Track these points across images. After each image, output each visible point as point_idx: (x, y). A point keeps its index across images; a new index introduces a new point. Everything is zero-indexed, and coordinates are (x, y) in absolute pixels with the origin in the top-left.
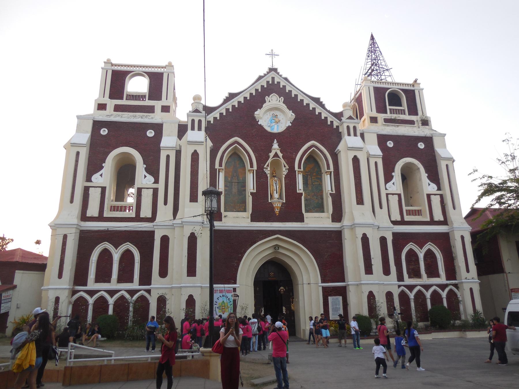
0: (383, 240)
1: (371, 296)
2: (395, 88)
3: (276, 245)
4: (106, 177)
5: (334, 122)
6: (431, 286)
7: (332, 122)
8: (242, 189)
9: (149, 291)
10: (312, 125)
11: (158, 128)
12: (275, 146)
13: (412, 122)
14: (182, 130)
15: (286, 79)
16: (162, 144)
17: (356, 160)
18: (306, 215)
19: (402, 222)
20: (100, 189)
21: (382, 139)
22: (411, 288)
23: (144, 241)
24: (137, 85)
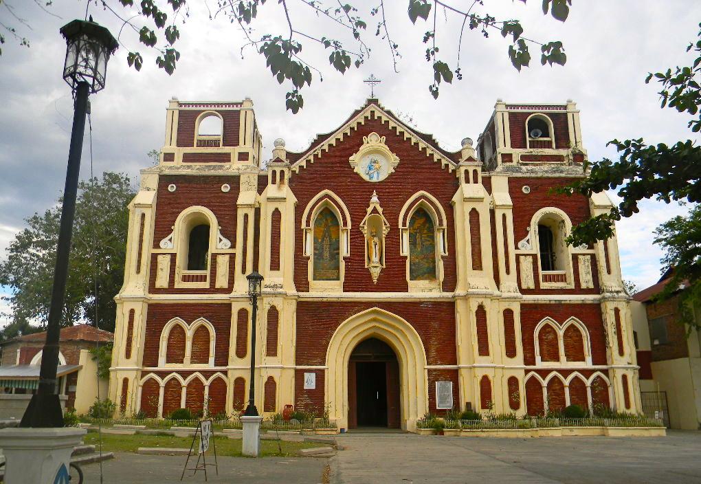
0: (508, 314)
2: (538, 112)
4: (176, 242)
5: (450, 165)
6: (571, 371)
7: (447, 166)
8: (335, 252)
9: (225, 373)
10: (423, 167)
11: (235, 181)
12: (375, 199)
13: (559, 158)
14: (262, 183)
15: (389, 113)
16: (238, 203)
17: (474, 214)
18: (411, 283)
19: (537, 290)
20: (169, 257)
21: (515, 185)
22: (544, 373)
23: (219, 314)
24: (210, 127)
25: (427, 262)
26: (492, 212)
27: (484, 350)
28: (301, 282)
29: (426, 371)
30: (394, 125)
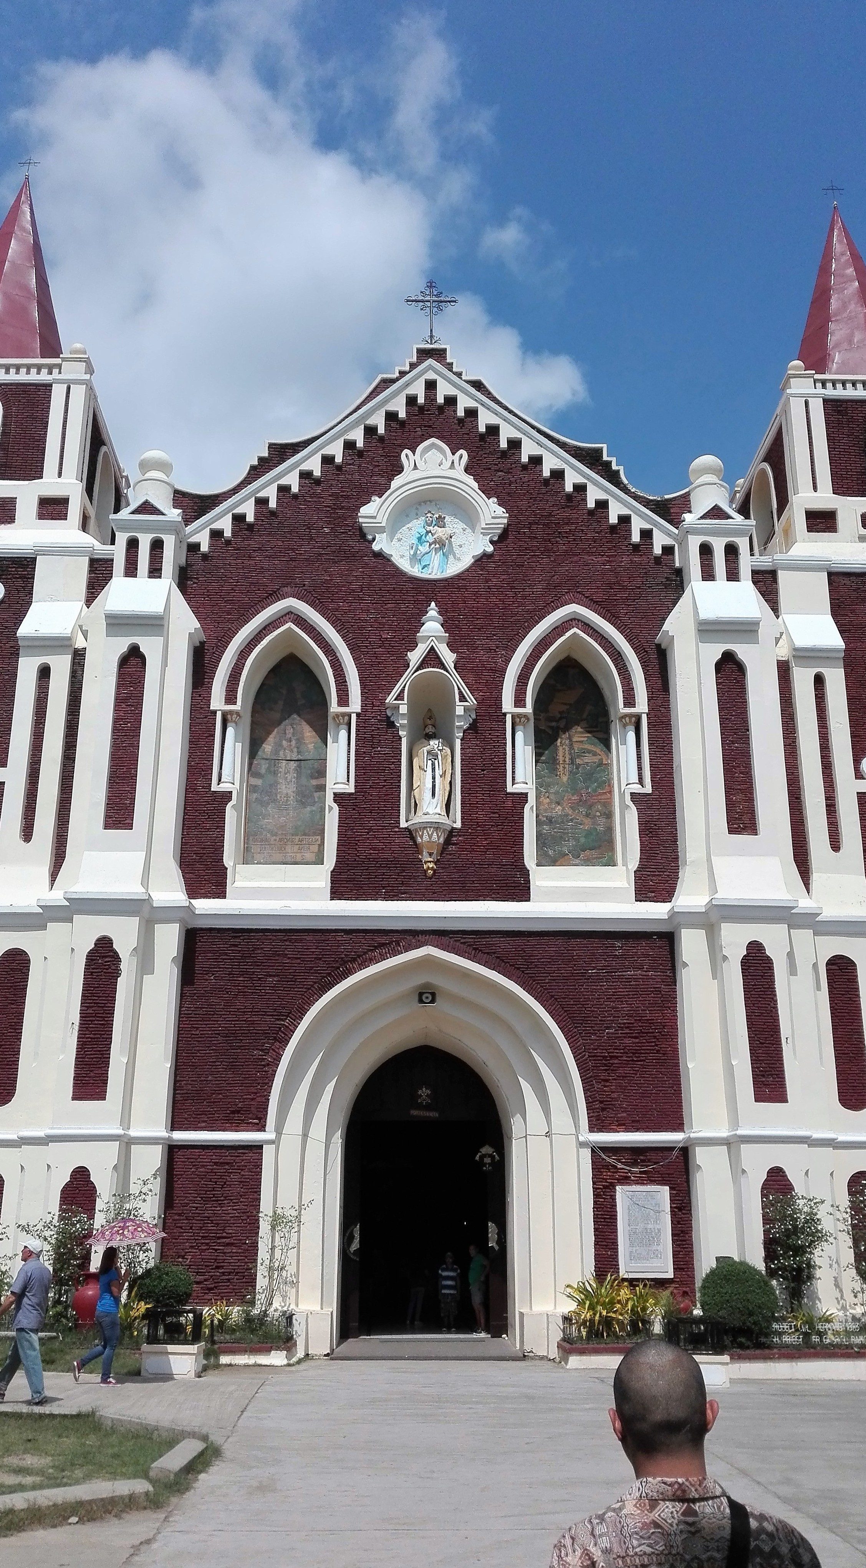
1: (777, 1183)
3: (427, 985)
8: (314, 782)
12: (432, 627)
15: (478, 385)
16: (27, 628)
17: (730, 670)
25: (587, 815)
26: (784, 670)
27: (769, 1082)
28: (203, 869)
29: (587, 1154)
30: (494, 420)
